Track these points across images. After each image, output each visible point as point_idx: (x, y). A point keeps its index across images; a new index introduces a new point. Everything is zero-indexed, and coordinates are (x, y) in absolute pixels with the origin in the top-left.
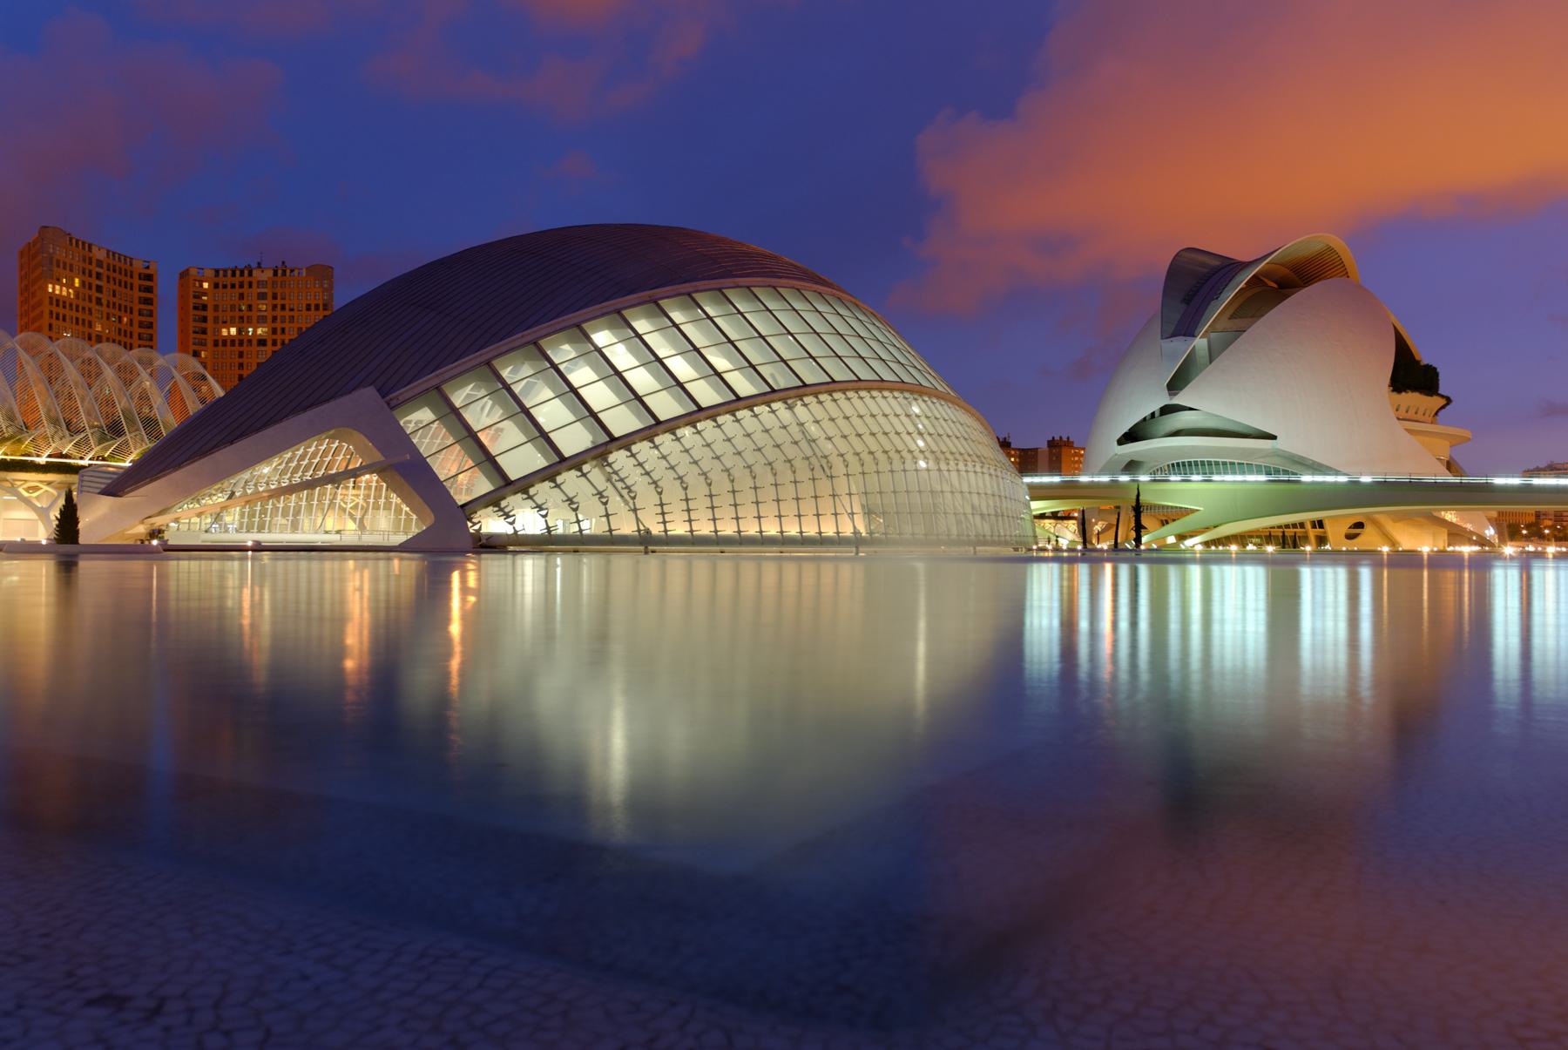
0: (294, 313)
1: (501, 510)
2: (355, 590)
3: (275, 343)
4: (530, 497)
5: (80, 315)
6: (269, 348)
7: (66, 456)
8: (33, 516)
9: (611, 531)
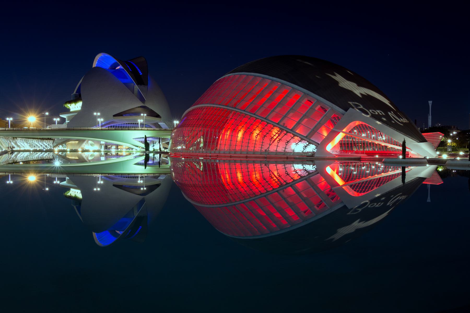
4: (299, 175)
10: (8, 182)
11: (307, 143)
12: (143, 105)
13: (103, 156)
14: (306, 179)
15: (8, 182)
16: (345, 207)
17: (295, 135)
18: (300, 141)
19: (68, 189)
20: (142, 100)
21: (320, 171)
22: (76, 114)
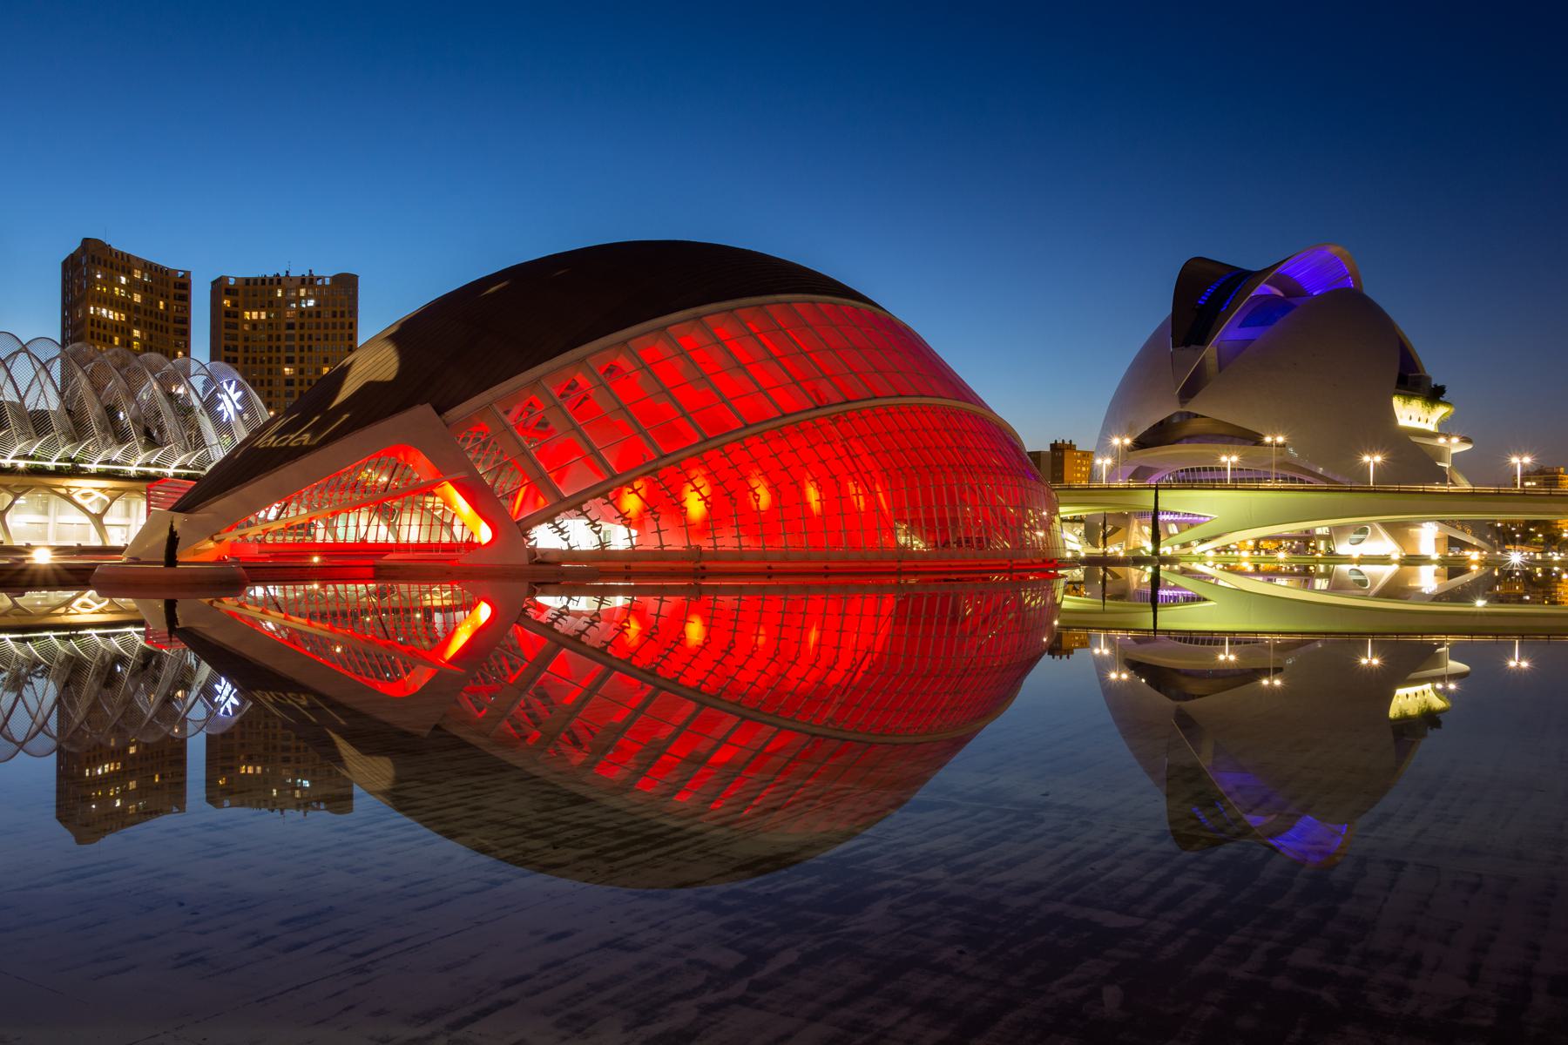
0: (314, 343)
1: (556, 526)
2: (310, 624)
3: (301, 383)
4: (584, 514)
5: (102, 331)
6: (296, 388)
7: (116, 463)
8: (86, 519)
9: (662, 546)
10: (1364, 661)
11: (556, 626)
12: (1184, 704)
13: (1322, 537)
14: (562, 500)
15: (1364, 661)
16: (440, 411)
17: (602, 651)
18: (583, 632)
19: (1445, 428)
20: (1186, 722)
21: (511, 529)
22: (1413, 675)
